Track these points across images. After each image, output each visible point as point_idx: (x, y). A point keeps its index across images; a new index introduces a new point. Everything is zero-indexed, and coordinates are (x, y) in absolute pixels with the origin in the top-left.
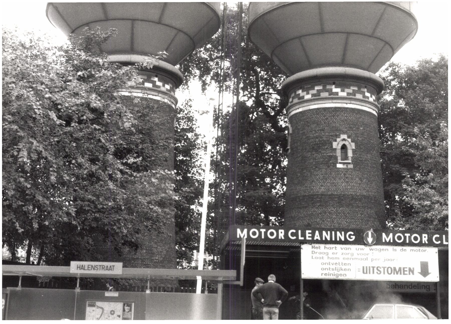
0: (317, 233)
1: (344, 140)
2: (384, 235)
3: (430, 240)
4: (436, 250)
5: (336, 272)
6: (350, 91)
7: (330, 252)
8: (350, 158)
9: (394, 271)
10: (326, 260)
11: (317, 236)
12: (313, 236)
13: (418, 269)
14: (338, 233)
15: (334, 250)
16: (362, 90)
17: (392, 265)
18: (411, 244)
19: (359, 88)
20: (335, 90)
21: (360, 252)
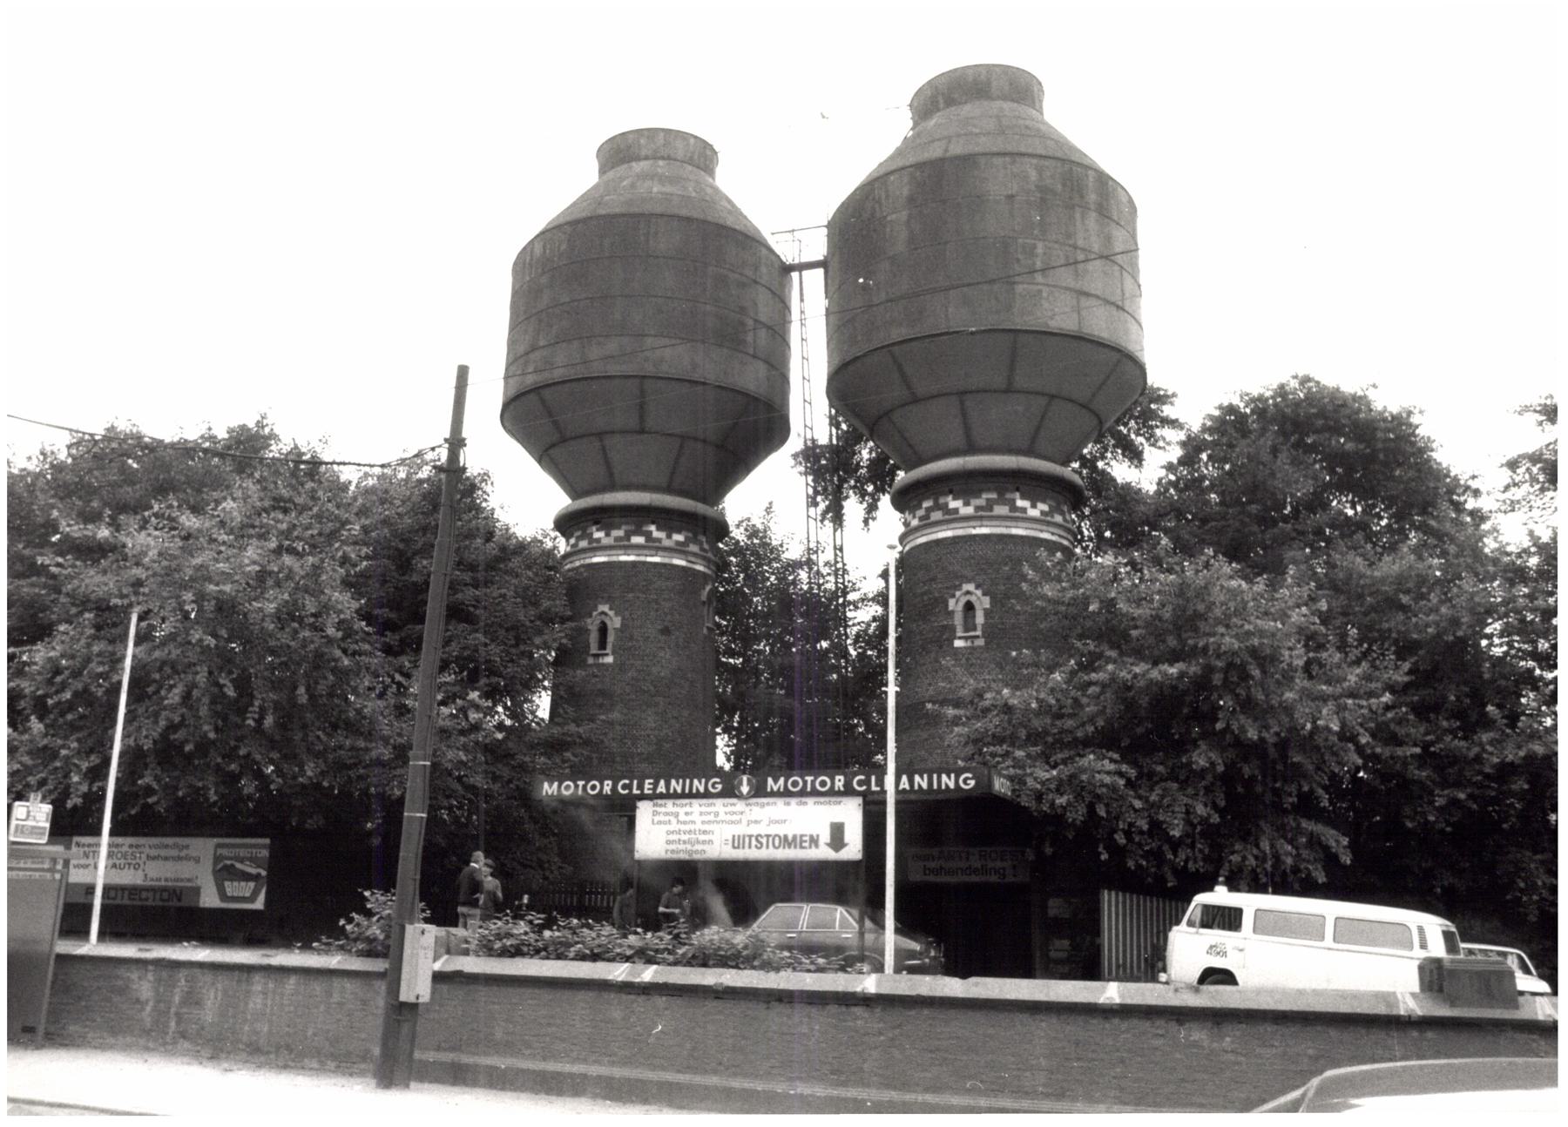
0: (662, 783)
1: (968, 593)
2: (770, 780)
3: (848, 784)
4: (859, 800)
5: (689, 847)
6: (981, 502)
7: (682, 811)
8: (979, 628)
9: (786, 842)
10: (674, 826)
11: (661, 788)
12: (655, 788)
13: (825, 836)
14: (944, 777)
15: (688, 809)
16: (1008, 496)
17: (781, 830)
18: (815, 793)
19: (1001, 494)
20: (954, 504)
21: (730, 809)
